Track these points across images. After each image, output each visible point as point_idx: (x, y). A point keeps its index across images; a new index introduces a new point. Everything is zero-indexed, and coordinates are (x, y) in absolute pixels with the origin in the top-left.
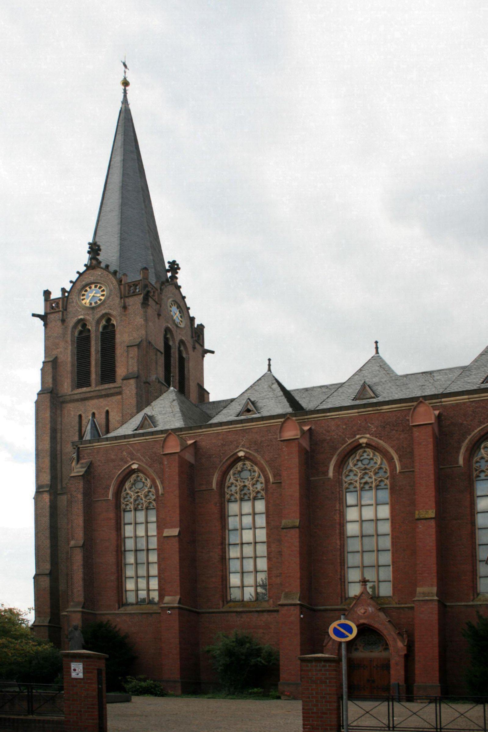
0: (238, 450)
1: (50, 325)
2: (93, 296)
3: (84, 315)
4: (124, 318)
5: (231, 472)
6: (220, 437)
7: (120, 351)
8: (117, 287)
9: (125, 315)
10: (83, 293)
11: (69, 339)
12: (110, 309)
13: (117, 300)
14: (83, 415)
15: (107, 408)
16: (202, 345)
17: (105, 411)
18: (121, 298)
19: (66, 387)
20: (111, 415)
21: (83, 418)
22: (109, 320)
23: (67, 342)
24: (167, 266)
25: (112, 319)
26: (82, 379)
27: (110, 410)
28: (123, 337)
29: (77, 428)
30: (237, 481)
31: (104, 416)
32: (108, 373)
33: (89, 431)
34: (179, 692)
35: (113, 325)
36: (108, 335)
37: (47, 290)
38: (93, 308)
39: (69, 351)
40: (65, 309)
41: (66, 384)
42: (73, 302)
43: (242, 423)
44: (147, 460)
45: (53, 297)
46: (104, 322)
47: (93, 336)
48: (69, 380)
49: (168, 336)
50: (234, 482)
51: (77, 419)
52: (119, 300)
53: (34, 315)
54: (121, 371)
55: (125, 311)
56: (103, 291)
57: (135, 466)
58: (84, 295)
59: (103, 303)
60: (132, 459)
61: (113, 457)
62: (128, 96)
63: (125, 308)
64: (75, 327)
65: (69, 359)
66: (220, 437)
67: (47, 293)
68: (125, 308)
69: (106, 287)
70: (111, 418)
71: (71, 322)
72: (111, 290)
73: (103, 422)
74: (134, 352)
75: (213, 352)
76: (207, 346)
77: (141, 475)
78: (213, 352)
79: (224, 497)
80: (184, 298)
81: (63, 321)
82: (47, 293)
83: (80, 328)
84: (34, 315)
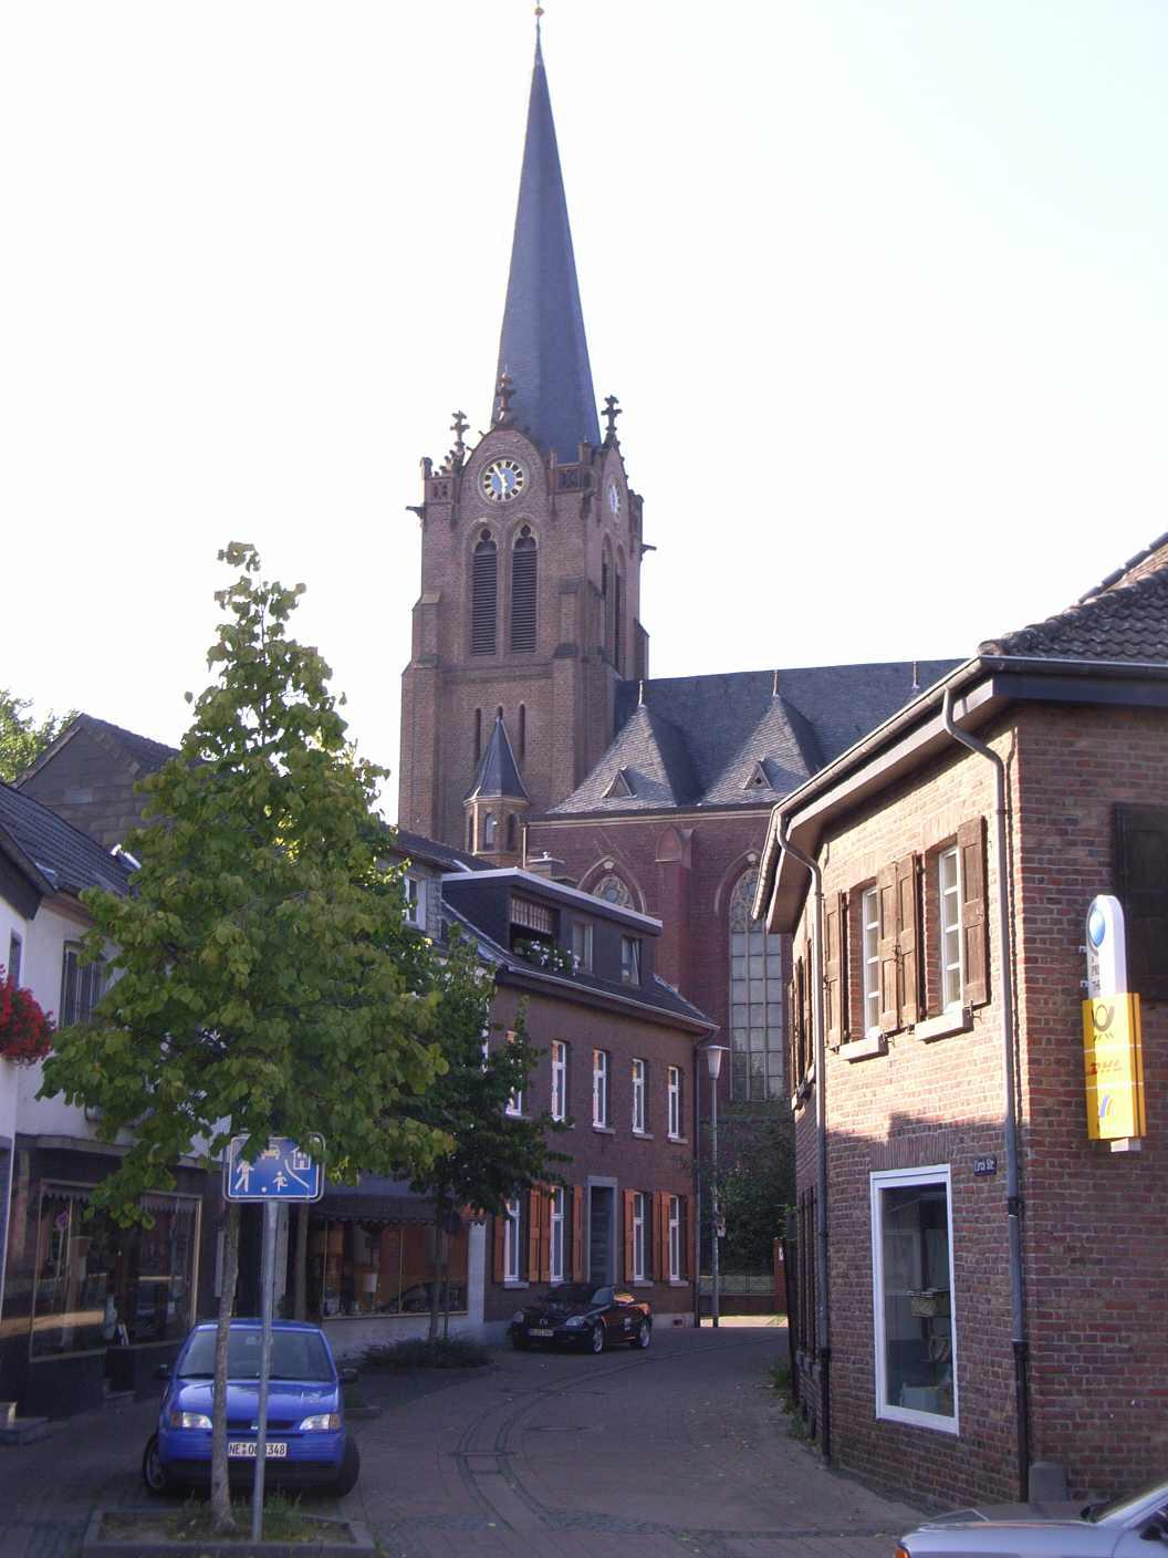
0: (748, 852)
1: (431, 528)
2: (503, 481)
3: (488, 516)
4: (553, 533)
5: (738, 884)
6: (726, 827)
7: (543, 595)
8: (542, 471)
9: (554, 528)
10: (488, 474)
11: (463, 560)
12: (530, 512)
13: (542, 496)
14: (483, 711)
15: (522, 702)
16: (641, 540)
17: (519, 706)
18: (548, 494)
19: (458, 651)
20: (528, 713)
21: (483, 716)
22: (526, 530)
23: (459, 564)
24: (601, 405)
25: (532, 529)
26: (481, 641)
27: (527, 707)
28: (549, 569)
29: (472, 734)
30: (744, 899)
31: (516, 717)
32: (523, 634)
33: (498, 747)
34: (893, 1293)
35: (532, 540)
36: (525, 564)
37: (428, 458)
38: (503, 507)
39: (463, 582)
40: (458, 499)
41: (456, 646)
42: (470, 488)
43: (754, 809)
44: (625, 855)
45: (435, 468)
46: (518, 535)
47: (501, 559)
48: (462, 641)
49: (606, 561)
50: (741, 901)
51: (473, 715)
52: (545, 496)
53: (408, 508)
54: (545, 635)
55: (553, 520)
56: (519, 475)
57: (609, 865)
58: (488, 478)
59: (521, 499)
60: (606, 853)
61: (578, 846)
62: (542, 43)
63: (554, 514)
64: (471, 537)
65: (462, 599)
66: (726, 827)
67: (427, 462)
68: (554, 514)
69: (517, 461)
70: (527, 720)
71: (467, 530)
72: (532, 476)
73: (516, 727)
74: (570, 604)
75: (654, 548)
76: (646, 541)
77: (616, 878)
78: (654, 548)
79: (728, 925)
80: (627, 477)
81: (454, 524)
82: (427, 462)
83: (480, 539)
84: (408, 508)
